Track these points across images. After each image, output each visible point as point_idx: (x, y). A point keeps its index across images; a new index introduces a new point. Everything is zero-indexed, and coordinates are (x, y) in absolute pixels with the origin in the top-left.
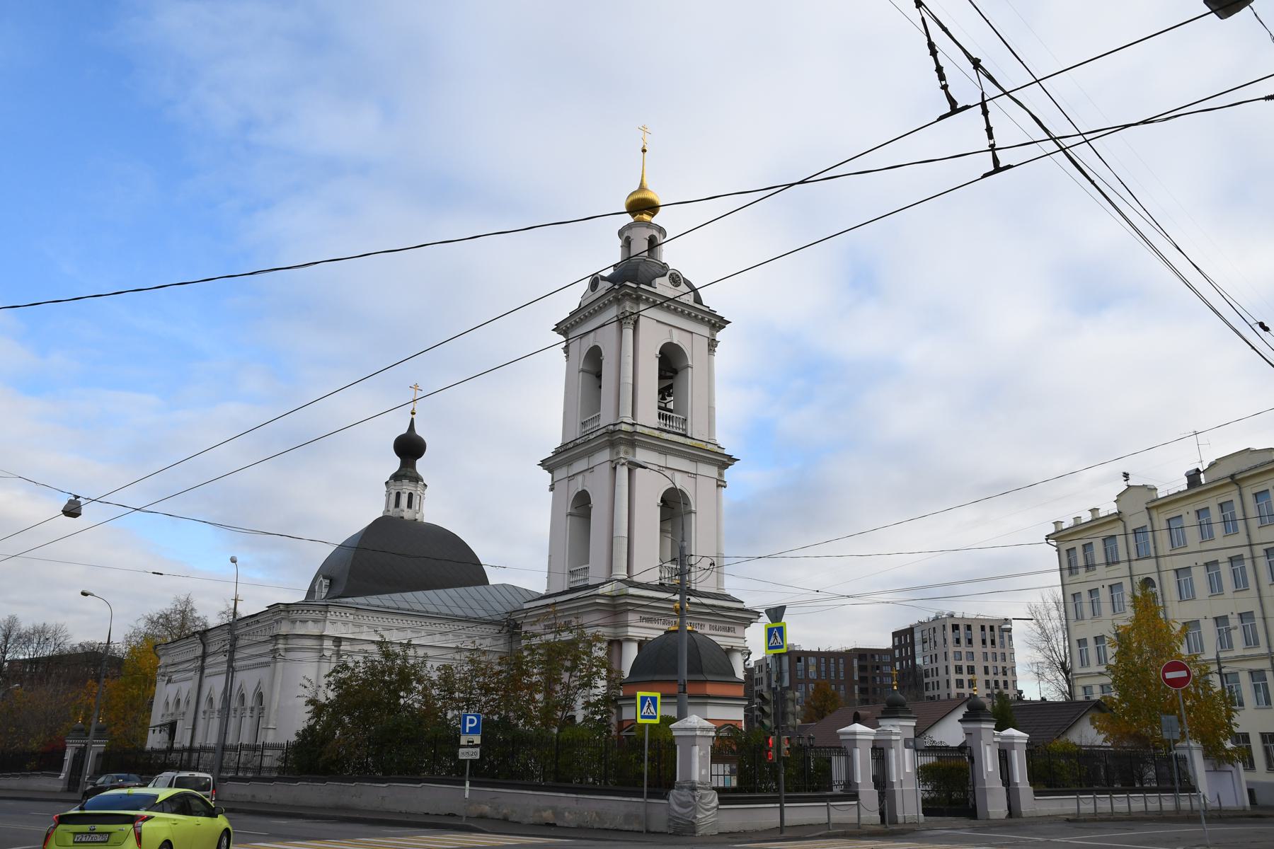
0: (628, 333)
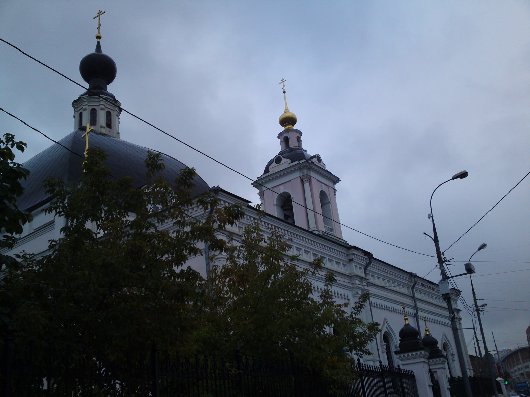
0: (307, 185)
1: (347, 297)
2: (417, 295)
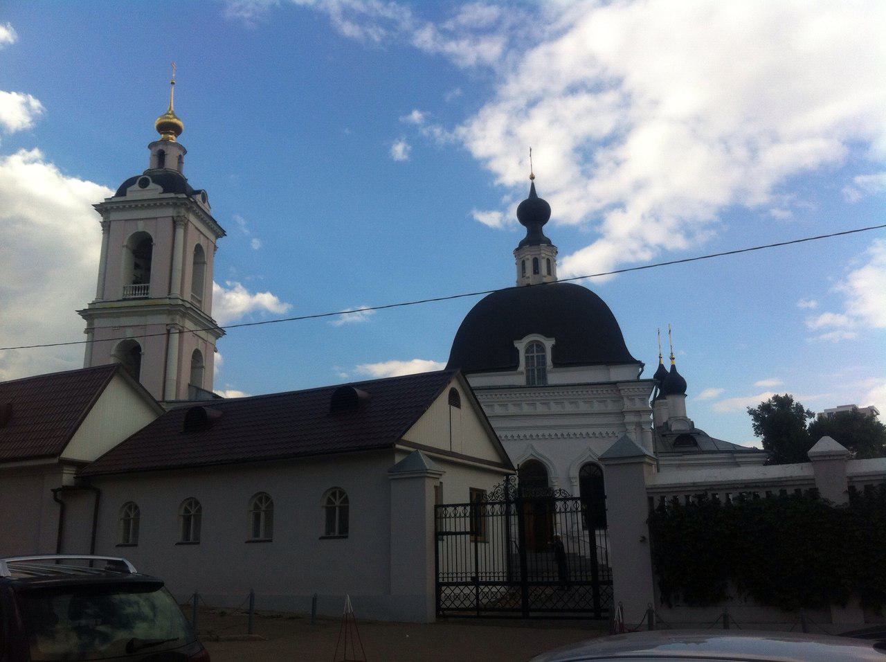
0: (180, 232)
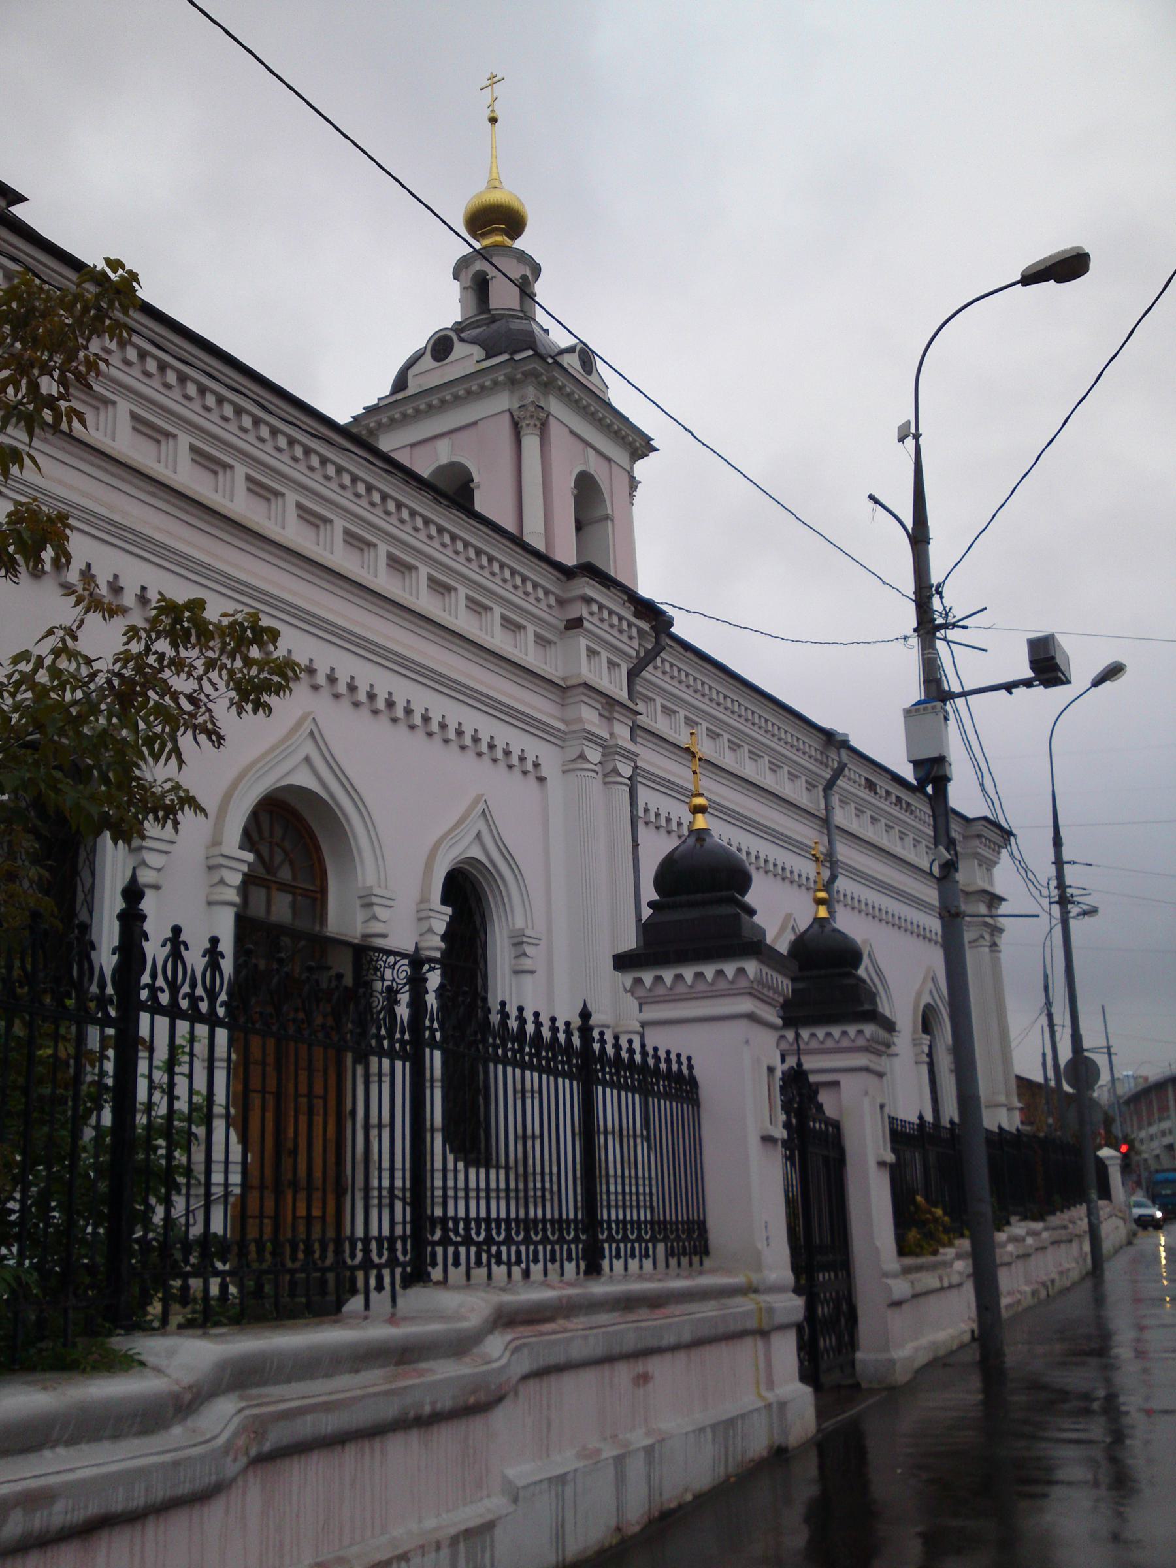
0: (531, 443)
1: (536, 765)
2: (840, 817)
